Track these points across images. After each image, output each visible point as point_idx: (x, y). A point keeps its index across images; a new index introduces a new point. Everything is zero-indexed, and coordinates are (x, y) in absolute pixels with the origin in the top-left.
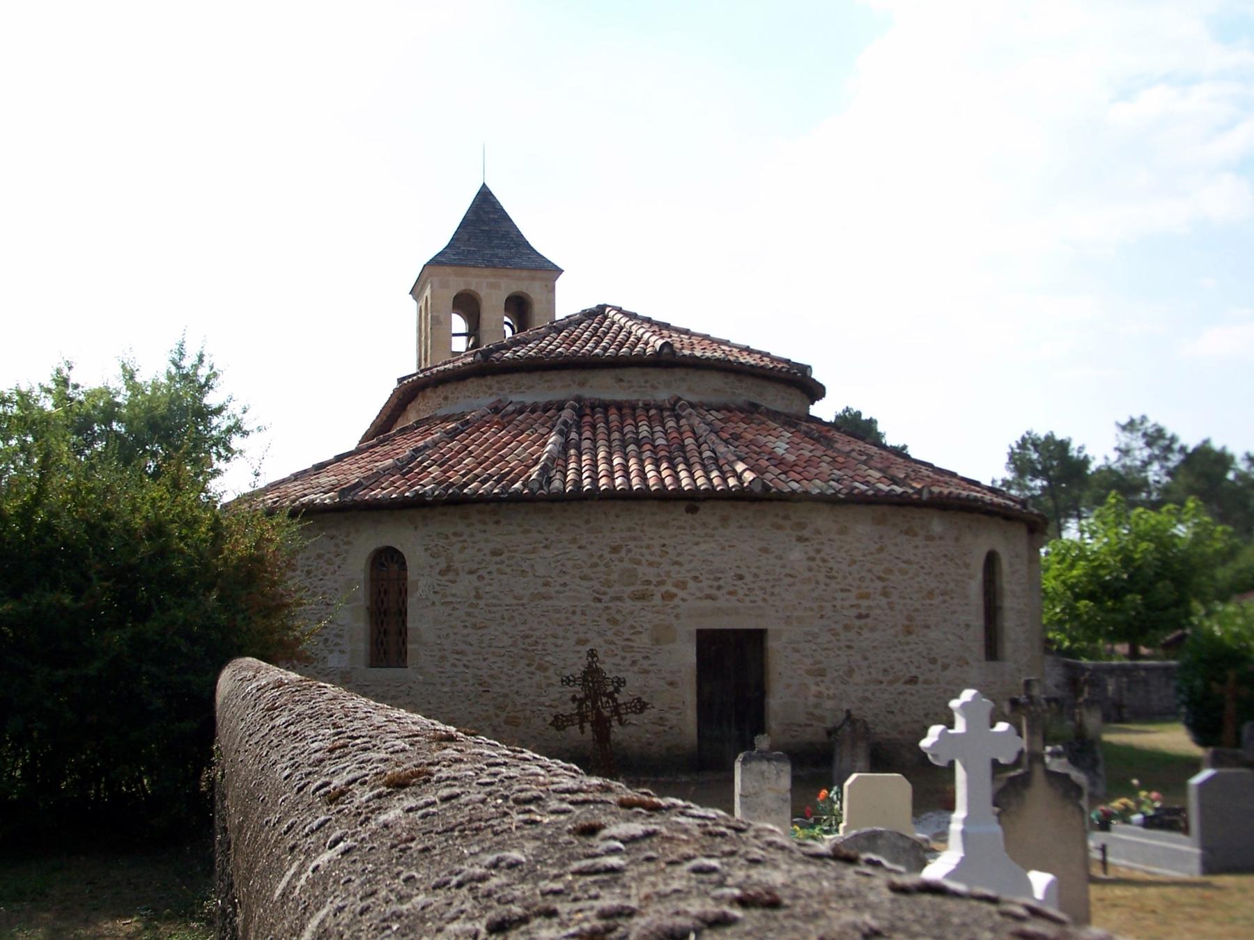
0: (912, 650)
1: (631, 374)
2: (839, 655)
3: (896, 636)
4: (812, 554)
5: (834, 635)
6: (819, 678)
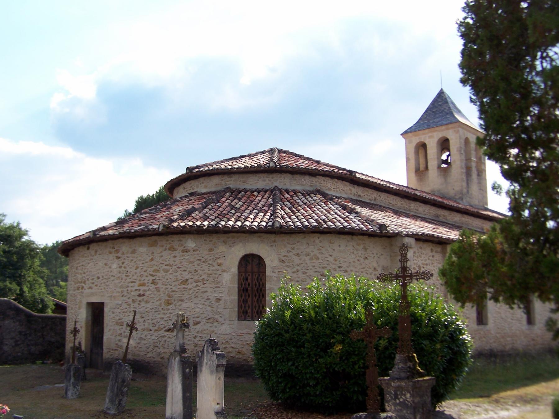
0: (170, 313)
1: (235, 177)
2: (129, 316)
3: (160, 305)
4: (121, 265)
5: (128, 305)
6: (121, 327)
